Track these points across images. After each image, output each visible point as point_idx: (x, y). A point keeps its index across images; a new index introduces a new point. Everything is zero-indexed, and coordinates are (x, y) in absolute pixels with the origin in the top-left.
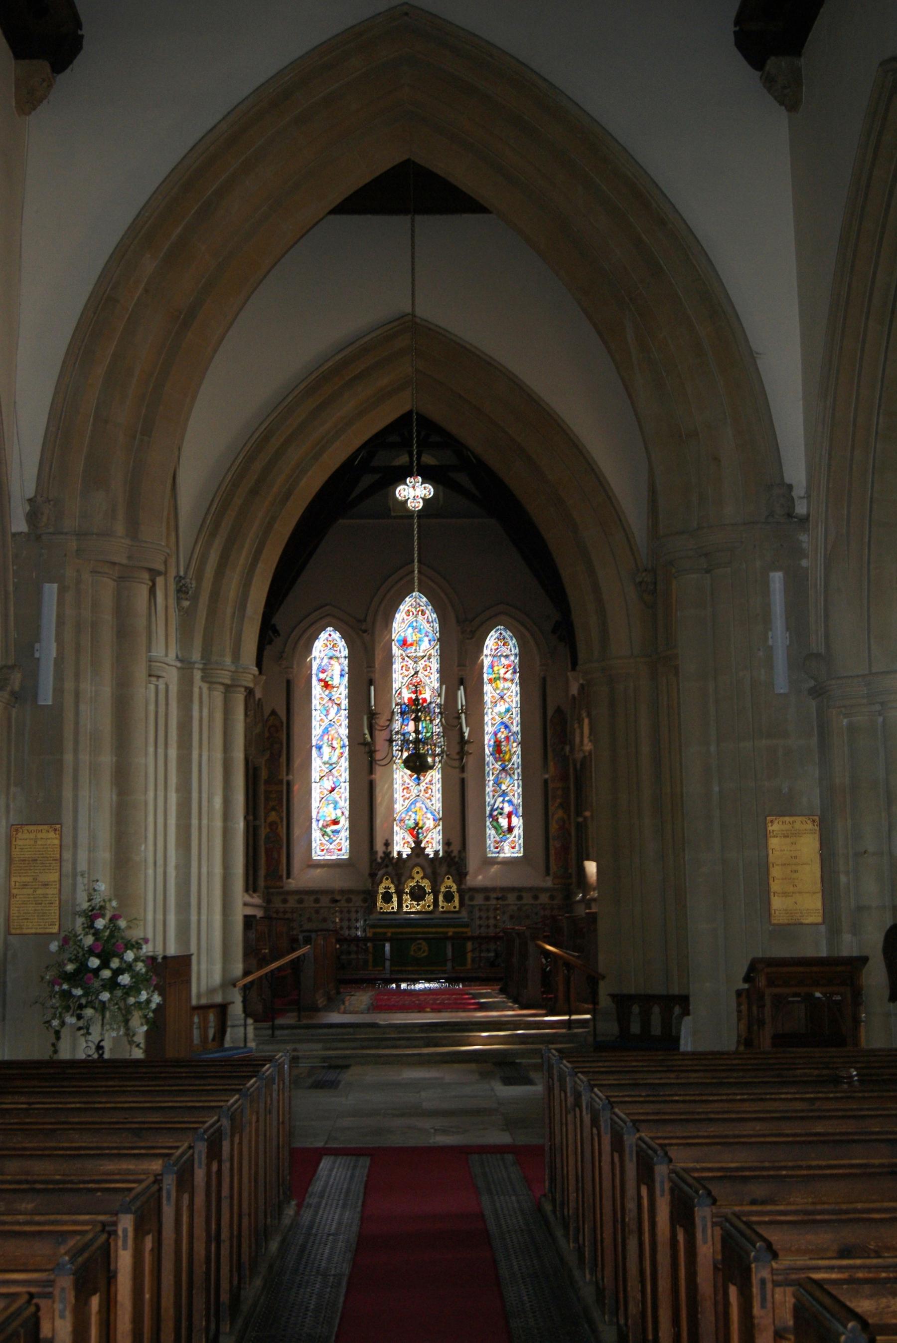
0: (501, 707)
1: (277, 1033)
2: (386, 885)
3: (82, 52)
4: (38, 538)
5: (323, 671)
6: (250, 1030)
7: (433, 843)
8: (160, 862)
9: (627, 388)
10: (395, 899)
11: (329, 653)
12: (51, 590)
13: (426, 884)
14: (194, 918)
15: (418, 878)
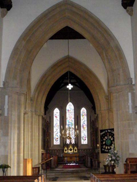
1: (47, 172)
2: (66, 148)
3: (12, 8)
4: (5, 88)
6: (43, 171)
7: (73, 142)
8: (28, 144)
9: (104, 63)
10: (67, 150)
11: (57, 112)
12: (7, 97)
13: (72, 148)
14: (33, 153)
15: (71, 147)
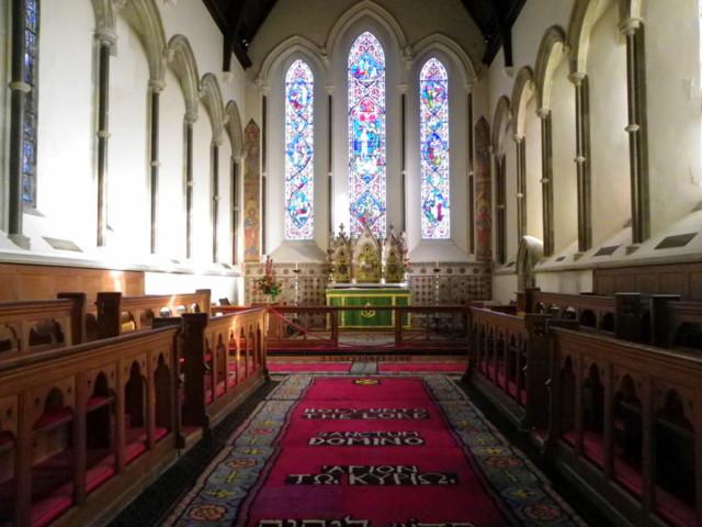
0: (433, 122)
5: (295, 94)
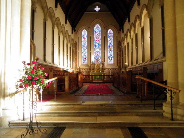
0: (110, 41)
